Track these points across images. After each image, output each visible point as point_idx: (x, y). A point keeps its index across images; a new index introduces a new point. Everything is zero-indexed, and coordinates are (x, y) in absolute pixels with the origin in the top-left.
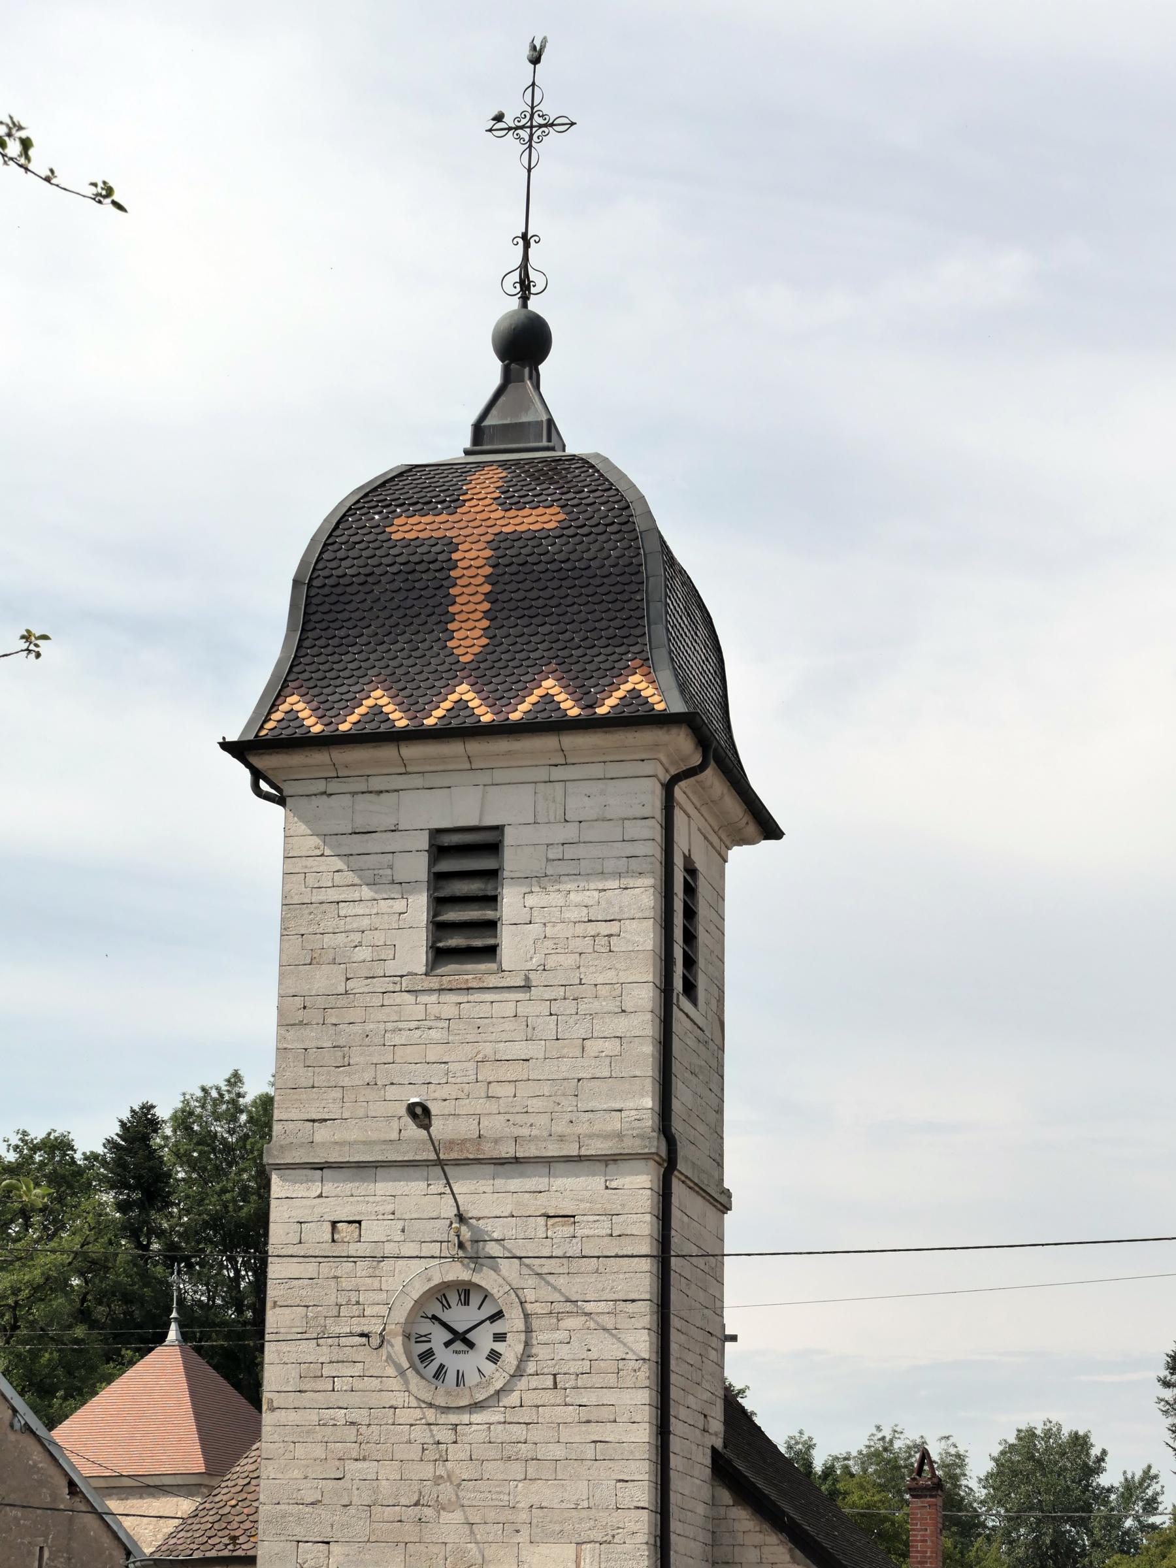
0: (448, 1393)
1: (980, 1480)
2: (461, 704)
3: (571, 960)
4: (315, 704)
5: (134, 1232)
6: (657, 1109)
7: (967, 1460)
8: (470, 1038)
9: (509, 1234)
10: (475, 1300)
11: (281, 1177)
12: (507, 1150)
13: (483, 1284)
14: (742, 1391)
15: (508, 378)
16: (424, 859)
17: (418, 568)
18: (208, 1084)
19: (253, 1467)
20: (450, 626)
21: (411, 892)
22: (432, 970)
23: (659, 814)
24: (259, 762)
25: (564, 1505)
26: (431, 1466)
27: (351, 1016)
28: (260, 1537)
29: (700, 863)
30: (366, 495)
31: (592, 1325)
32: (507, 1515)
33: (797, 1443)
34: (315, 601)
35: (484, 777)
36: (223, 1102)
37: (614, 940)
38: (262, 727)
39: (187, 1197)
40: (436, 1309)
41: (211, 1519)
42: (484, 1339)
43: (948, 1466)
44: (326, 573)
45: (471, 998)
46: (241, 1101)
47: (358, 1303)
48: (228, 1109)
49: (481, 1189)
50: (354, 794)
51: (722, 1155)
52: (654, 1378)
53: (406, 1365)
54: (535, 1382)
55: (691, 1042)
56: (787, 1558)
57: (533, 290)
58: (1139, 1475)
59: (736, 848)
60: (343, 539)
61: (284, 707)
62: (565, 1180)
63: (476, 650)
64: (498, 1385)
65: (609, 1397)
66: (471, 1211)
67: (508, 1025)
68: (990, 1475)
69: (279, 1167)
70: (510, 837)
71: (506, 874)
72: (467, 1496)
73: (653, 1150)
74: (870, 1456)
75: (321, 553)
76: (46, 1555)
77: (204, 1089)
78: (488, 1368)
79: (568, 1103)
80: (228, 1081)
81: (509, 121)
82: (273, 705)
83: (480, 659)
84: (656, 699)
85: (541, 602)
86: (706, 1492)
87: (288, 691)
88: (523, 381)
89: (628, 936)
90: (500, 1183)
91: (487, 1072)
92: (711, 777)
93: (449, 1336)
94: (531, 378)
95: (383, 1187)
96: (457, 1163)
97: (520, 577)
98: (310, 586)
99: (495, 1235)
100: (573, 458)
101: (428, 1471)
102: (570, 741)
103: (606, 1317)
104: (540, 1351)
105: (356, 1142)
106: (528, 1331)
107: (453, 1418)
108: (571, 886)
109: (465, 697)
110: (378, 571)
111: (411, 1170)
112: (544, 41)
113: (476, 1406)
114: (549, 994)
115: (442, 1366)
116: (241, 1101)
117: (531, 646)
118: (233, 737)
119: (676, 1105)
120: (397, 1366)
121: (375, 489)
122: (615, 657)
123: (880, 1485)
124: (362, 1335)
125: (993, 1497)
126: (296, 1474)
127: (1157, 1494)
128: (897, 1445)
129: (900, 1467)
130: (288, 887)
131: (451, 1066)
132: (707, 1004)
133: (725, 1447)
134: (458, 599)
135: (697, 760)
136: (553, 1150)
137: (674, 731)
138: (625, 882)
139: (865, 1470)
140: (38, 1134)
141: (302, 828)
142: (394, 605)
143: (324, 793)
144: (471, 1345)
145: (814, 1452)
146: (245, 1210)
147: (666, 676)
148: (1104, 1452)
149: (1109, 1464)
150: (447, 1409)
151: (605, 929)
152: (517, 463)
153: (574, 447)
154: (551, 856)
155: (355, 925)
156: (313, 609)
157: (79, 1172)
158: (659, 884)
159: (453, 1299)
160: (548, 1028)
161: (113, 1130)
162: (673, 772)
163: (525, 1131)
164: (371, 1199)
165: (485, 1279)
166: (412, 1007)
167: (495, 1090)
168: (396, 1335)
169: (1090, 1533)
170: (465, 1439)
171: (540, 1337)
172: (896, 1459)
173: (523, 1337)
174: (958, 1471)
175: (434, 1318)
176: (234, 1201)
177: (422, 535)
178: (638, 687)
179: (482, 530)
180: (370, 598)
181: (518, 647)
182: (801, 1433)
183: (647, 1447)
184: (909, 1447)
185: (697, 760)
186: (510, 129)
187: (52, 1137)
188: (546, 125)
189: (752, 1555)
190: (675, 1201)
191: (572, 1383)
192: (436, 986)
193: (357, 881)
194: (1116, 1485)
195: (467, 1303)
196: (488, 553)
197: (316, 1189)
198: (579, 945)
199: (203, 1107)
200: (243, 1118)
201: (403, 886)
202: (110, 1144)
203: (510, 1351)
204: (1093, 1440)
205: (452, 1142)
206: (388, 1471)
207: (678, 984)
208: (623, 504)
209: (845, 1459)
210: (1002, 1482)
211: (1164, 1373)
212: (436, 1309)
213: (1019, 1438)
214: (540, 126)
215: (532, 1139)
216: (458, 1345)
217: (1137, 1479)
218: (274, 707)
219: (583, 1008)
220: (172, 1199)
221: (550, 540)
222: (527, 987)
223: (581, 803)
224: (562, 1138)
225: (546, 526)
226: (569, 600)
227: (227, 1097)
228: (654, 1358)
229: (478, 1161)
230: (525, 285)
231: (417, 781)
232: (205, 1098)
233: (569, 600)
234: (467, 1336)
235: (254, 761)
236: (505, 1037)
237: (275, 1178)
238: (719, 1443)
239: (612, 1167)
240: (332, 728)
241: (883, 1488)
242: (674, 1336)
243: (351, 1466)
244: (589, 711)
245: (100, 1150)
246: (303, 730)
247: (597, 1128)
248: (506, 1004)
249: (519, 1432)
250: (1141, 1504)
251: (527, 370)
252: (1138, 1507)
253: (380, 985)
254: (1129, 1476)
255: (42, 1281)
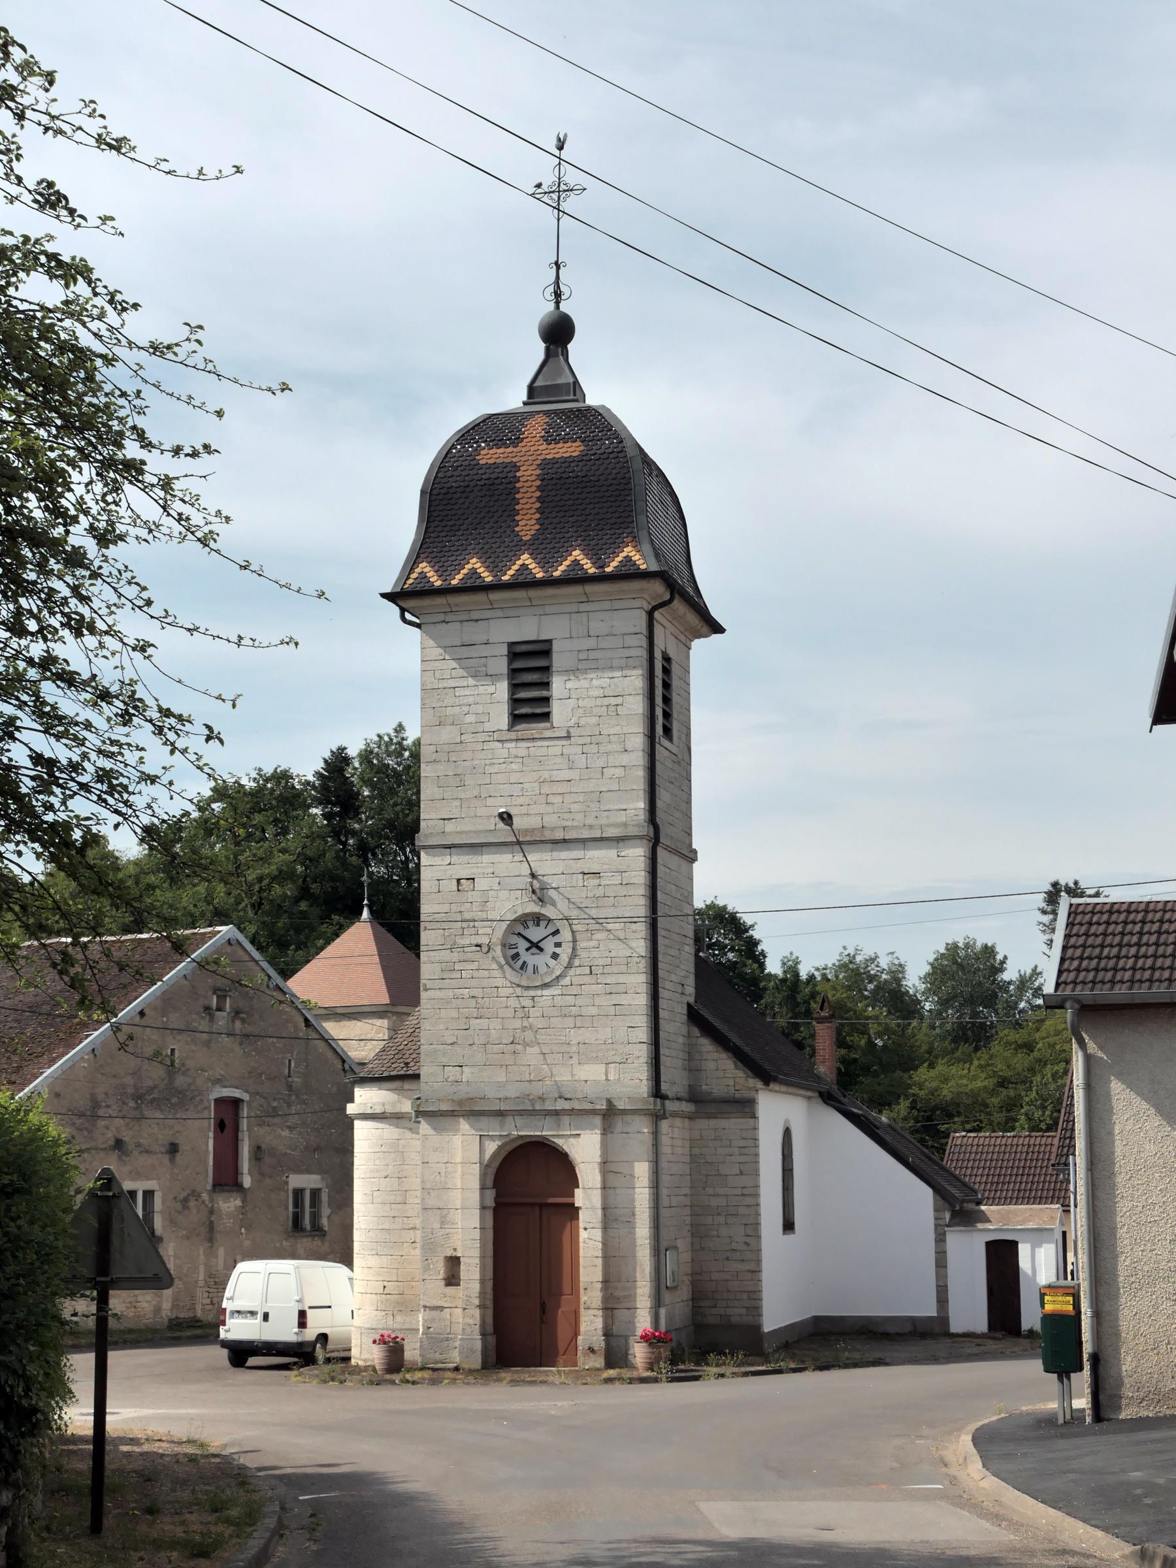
0: (528, 978)
1: (921, 978)
2: (524, 567)
3: (594, 720)
4: (436, 568)
5: (336, 834)
6: (647, 808)
7: (906, 968)
8: (535, 768)
9: (562, 884)
10: (543, 924)
11: (426, 853)
12: (559, 835)
13: (547, 914)
14: (752, 926)
15: (549, 354)
16: (505, 661)
17: (496, 481)
18: (382, 732)
19: (416, 1022)
20: (516, 518)
21: (498, 681)
22: (512, 727)
23: (644, 630)
24: (406, 604)
25: (598, 1042)
26: (520, 1020)
27: (465, 756)
28: (421, 1063)
29: (672, 654)
30: (463, 435)
31: (612, 937)
32: (565, 1048)
33: (789, 961)
34: (434, 503)
35: (540, 611)
36: (392, 744)
37: (619, 708)
38: (405, 583)
39: (371, 809)
40: (520, 929)
41: (393, 1053)
42: (549, 946)
43: (893, 972)
44: (440, 486)
45: (535, 744)
46: (405, 743)
47: (474, 927)
48: (396, 749)
49: (545, 858)
50: (462, 622)
51: (691, 828)
52: (649, 967)
53: (503, 962)
54: (579, 970)
55: (669, 764)
56: (733, 1066)
57: (563, 297)
58: (1029, 971)
59: (696, 640)
60: (450, 464)
61: (418, 570)
62: (594, 852)
63: (533, 532)
64: (558, 973)
65: (622, 978)
66: (539, 871)
67: (558, 760)
68: (928, 974)
69: (425, 847)
70: (556, 647)
71: (554, 669)
72: (541, 1037)
73: (645, 833)
74: (841, 966)
75: (437, 473)
76: (293, 1064)
77: (379, 736)
78: (552, 962)
79: (594, 806)
80: (395, 730)
81: (545, 188)
82: (411, 569)
83: (535, 538)
84: (641, 561)
85: (570, 502)
86: (684, 1030)
87: (420, 559)
88: (558, 356)
89: (628, 705)
90: (555, 854)
91: (546, 789)
92: (677, 604)
93: (528, 945)
94: (562, 355)
95: (487, 858)
96: (530, 843)
97: (558, 487)
98: (431, 494)
99: (554, 885)
100: (589, 408)
101: (518, 1024)
102: (590, 588)
103: (620, 932)
104: (583, 954)
105: (470, 832)
106: (574, 941)
107: (532, 993)
108: (593, 675)
109: (526, 562)
110: (472, 484)
111: (504, 848)
112: (566, 136)
113: (545, 986)
114: (581, 741)
115: (525, 962)
116: (405, 743)
117: (565, 530)
118: (388, 589)
119: (659, 804)
120: (498, 963)
121: (469, 431)
122: (616, 536)
123: (848, 986)
124: (477, 946)
125: (930, 990)
126: (441, 1027)
127: (1042, 985)
128: (859, 959)
129: (861, 974)
130: (424, 679)
131: (525, 786)
132: (679, 738)
133: (696, 1002)
134: (521, 490)
135: (667, 597)
136: (586, 834)
137: (652, 581)
138: (625, 672)
139: (837, 977)
140: (268, 770)
141: (432, 643)
142: (483, 504)
143: (444, 621)
144: (541, 950)
145: (800, 967)
146: (410, 817)
147: (647, 547)
148: (1005, 957)
149: (1009, 965)
150: (528, 988)
151: (613, 701)
152: (555, 412)
153: (592, 400)
154: (581, 658)
155: (465, 702)
156: (433, 508)
157: (297, 795)
158: (646, 673)
159: (530, 924)
160: (581, 761)
161: (319, 766)
162: (654, 603)
163: (569, 823)
164: (480, 865)
165: (548, 911)
166: (501, 750)
167: (551, 799)
168: (497, 945)
169: (997, 1014)
170: (540, 1005)
171: (581, 944)
172: (858, 969)
173: (571, 945)
174: (900, 975)
175: (519, 934)
176: (403, 810)
177: (498, 461)
178: (630, 554)
179: (534, 457)
180: (468, 501)
181: (558, 530)
182: (791, 953)
183: (645, 1007)
184: (867, 960)
185: (667, 597)
186: (545, 193)
187: (278, 770)
188: (568, 190)
189: (711, 1065)
190: (660, 860)
191: (601, 971)
192: (514, 738)
193: (465, 674)
194: (1014, 979)
195: (538, 925)
196: (538, 472)
197: (447, 860)
198: (597, 711)
199: (379, 747)
200: (407, 754)
201: (493, 677)
202: (318, 774)
203: (565, 952)
204: (998, 949)
205: (526, 830)
206: (496, 1024)
207: (659, 730)
208: (619, 440)
209: (824, 969)
210: (936, 979)
211: (1043, 905)
212: (520, 929)
213: (947, 949)
214: (565, 191)
215: (573, 827)
216: (534, 950)
217: (1027, 975)
218: (412, 570)
219: (602, 749)
220: (361, 810)
221: (575, 464)
222: (568, 737)
223: (599, 625)
224: (591, 827)
225: (573, 454)
226: (587, 501)
227: (395, 741)
228: (649, 955)
229: (542, 842)
230: (558, 295)
231: (499, 613)
232: (380, 741)
233: (587, 501)
234: (540, 944)
235: (401, 603)
236: (556, 767)
237: (422, 854)
238: (692, 1000)
239: (621, 844)
240: (447, 582)
241: (849, 988)
242: (660, 941)
243: (473, 1022)
244: (601, 570)
245: (311, 778)
246: (430, 584)
247: (611, 821)
248: (556, 748)
249: (570, 1000)
250: (1031, 991)
251: (560, 350)
252: (1029, 994)
253: (482, 737)
254: (1022, 973)
255: (277, 873)
